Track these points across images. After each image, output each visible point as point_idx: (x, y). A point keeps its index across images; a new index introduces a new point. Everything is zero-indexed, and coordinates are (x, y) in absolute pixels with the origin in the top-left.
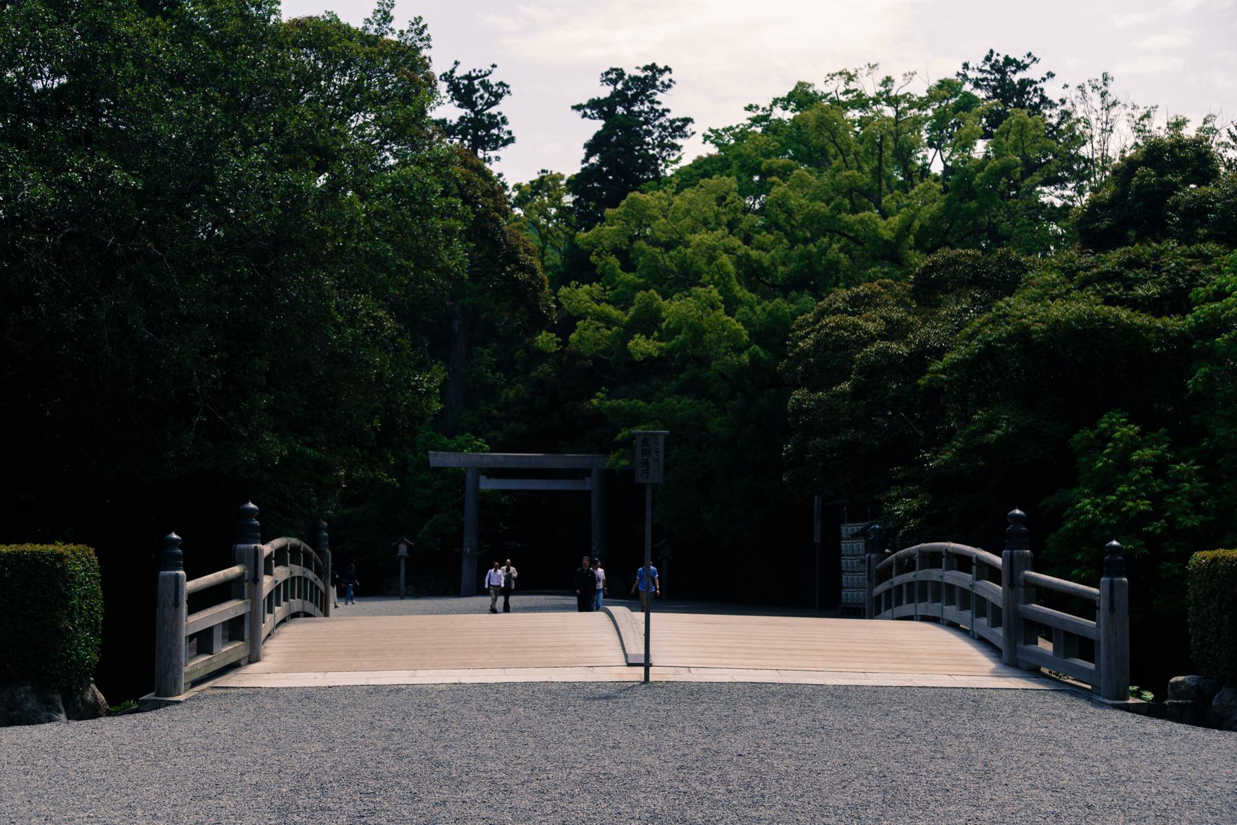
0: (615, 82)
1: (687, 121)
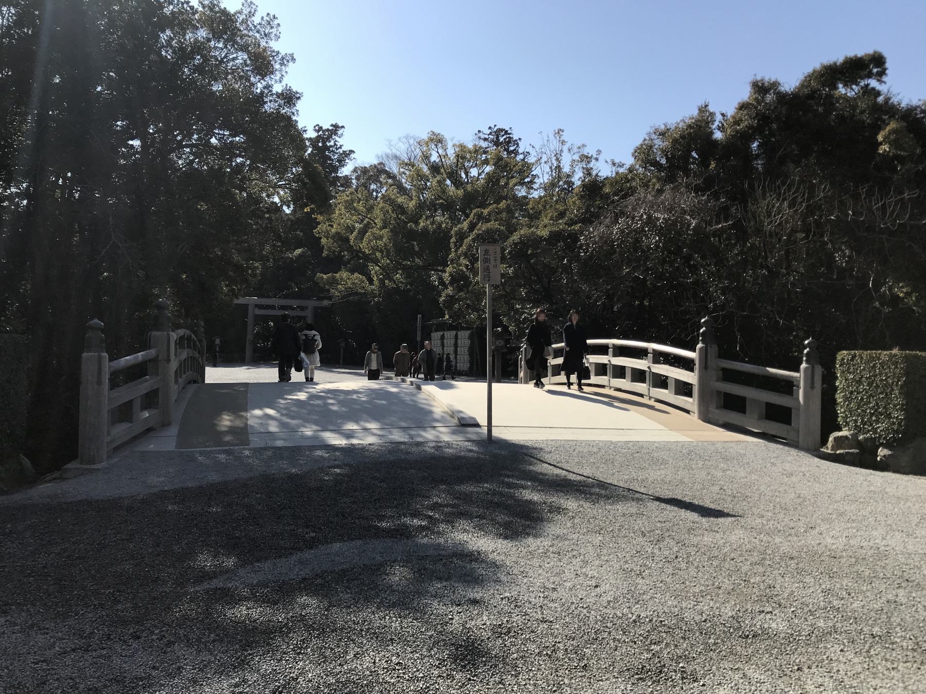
0: (318, 131)
1: (352, 152)
